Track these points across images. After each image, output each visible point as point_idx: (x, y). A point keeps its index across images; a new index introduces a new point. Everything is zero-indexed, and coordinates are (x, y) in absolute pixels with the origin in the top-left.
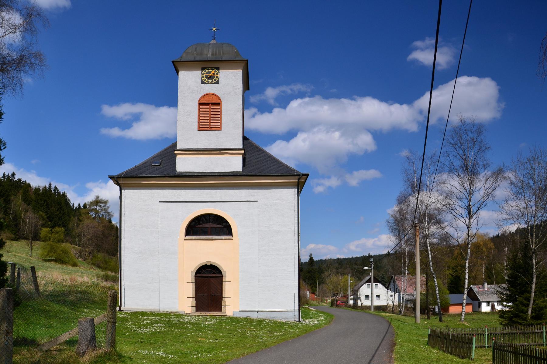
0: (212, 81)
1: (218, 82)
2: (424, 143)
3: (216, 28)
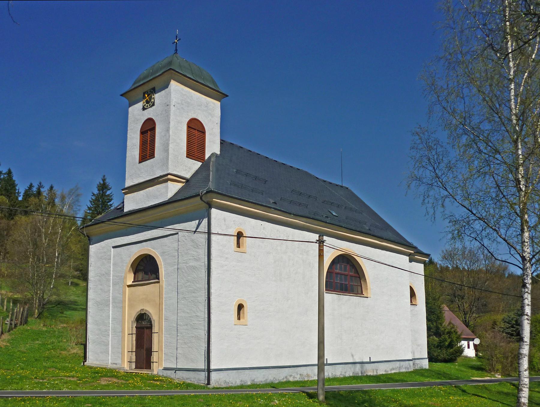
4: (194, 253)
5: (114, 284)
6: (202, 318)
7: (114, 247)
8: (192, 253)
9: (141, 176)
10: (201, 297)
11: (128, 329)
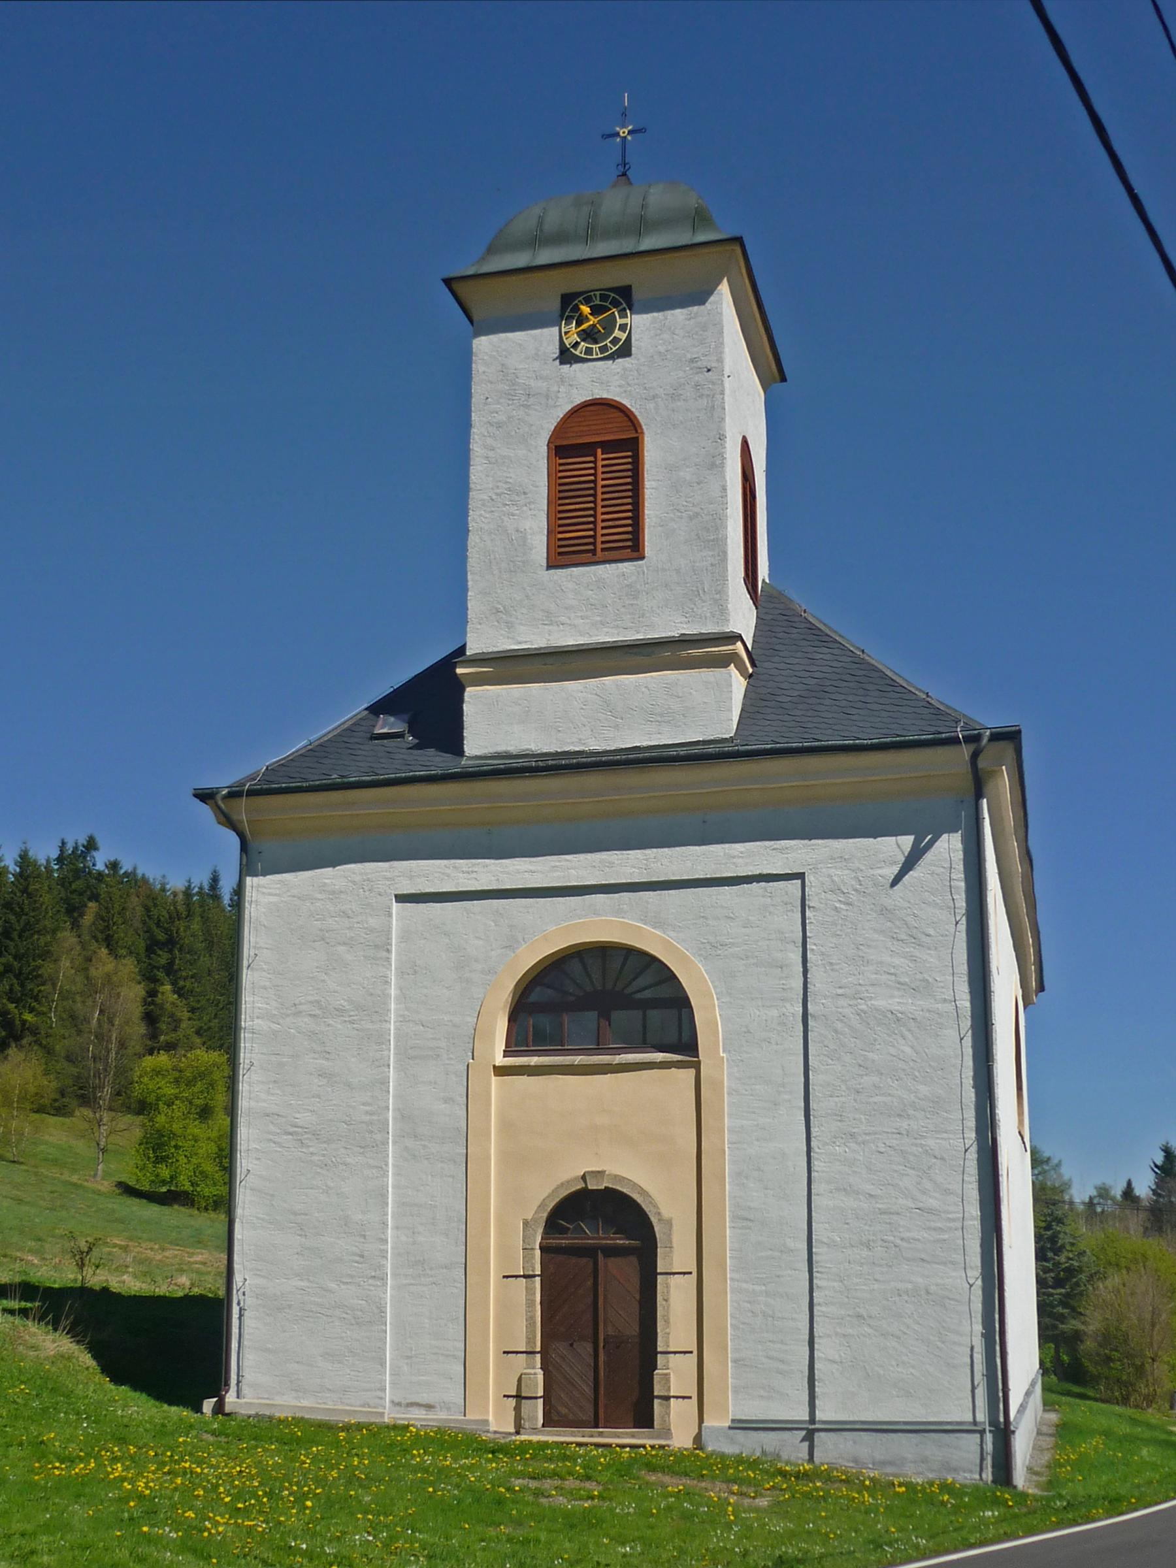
0: (603, 349)
1: (625, 350)
2: (1085, 113)
3: (630, 128)
4: (897, 961)
5: (408, 1056)
6: (953, 1220)
7: (401, 898)
8: (887, 958)
9: (563, 619)
10: (945, 1135)
11: (503, 1248)
